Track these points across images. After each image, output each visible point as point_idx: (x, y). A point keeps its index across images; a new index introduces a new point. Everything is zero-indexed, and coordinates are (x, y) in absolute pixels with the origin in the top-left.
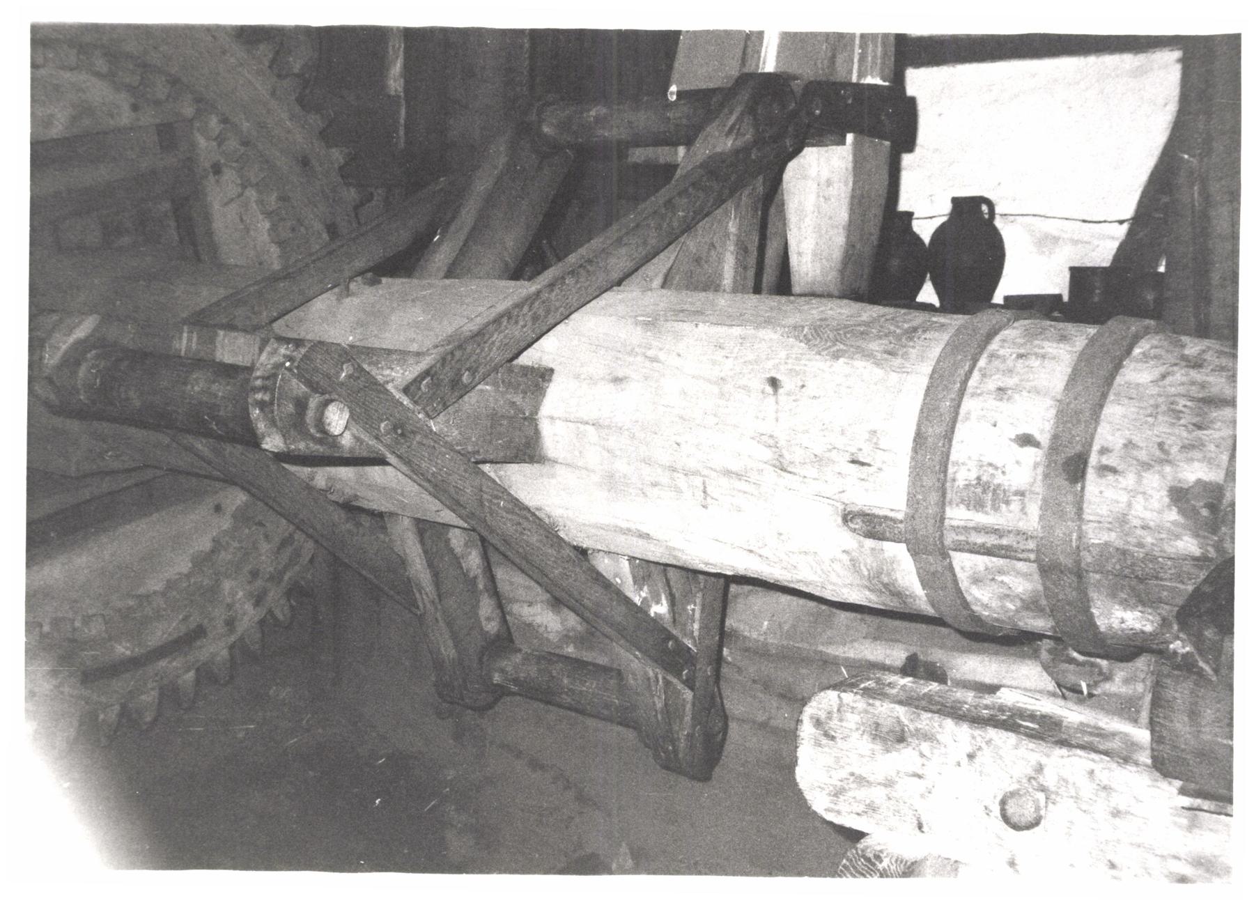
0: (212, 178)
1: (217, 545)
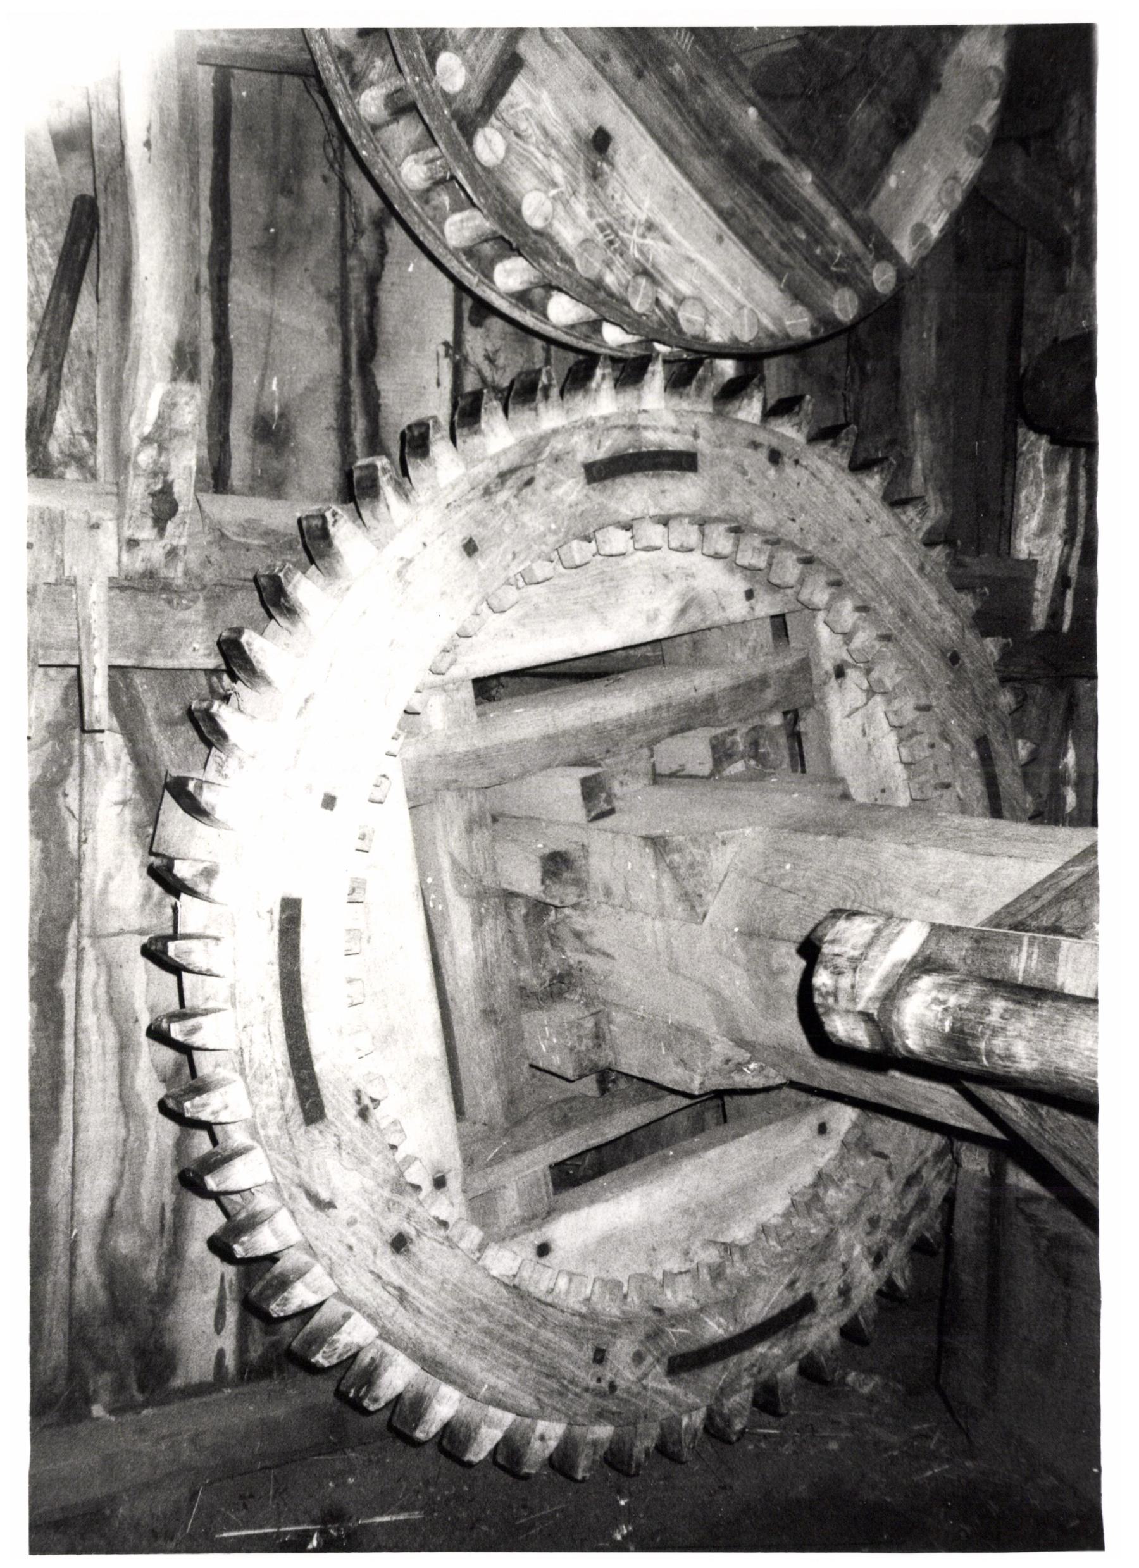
0: (833, 682)
1: (822, 1179)
